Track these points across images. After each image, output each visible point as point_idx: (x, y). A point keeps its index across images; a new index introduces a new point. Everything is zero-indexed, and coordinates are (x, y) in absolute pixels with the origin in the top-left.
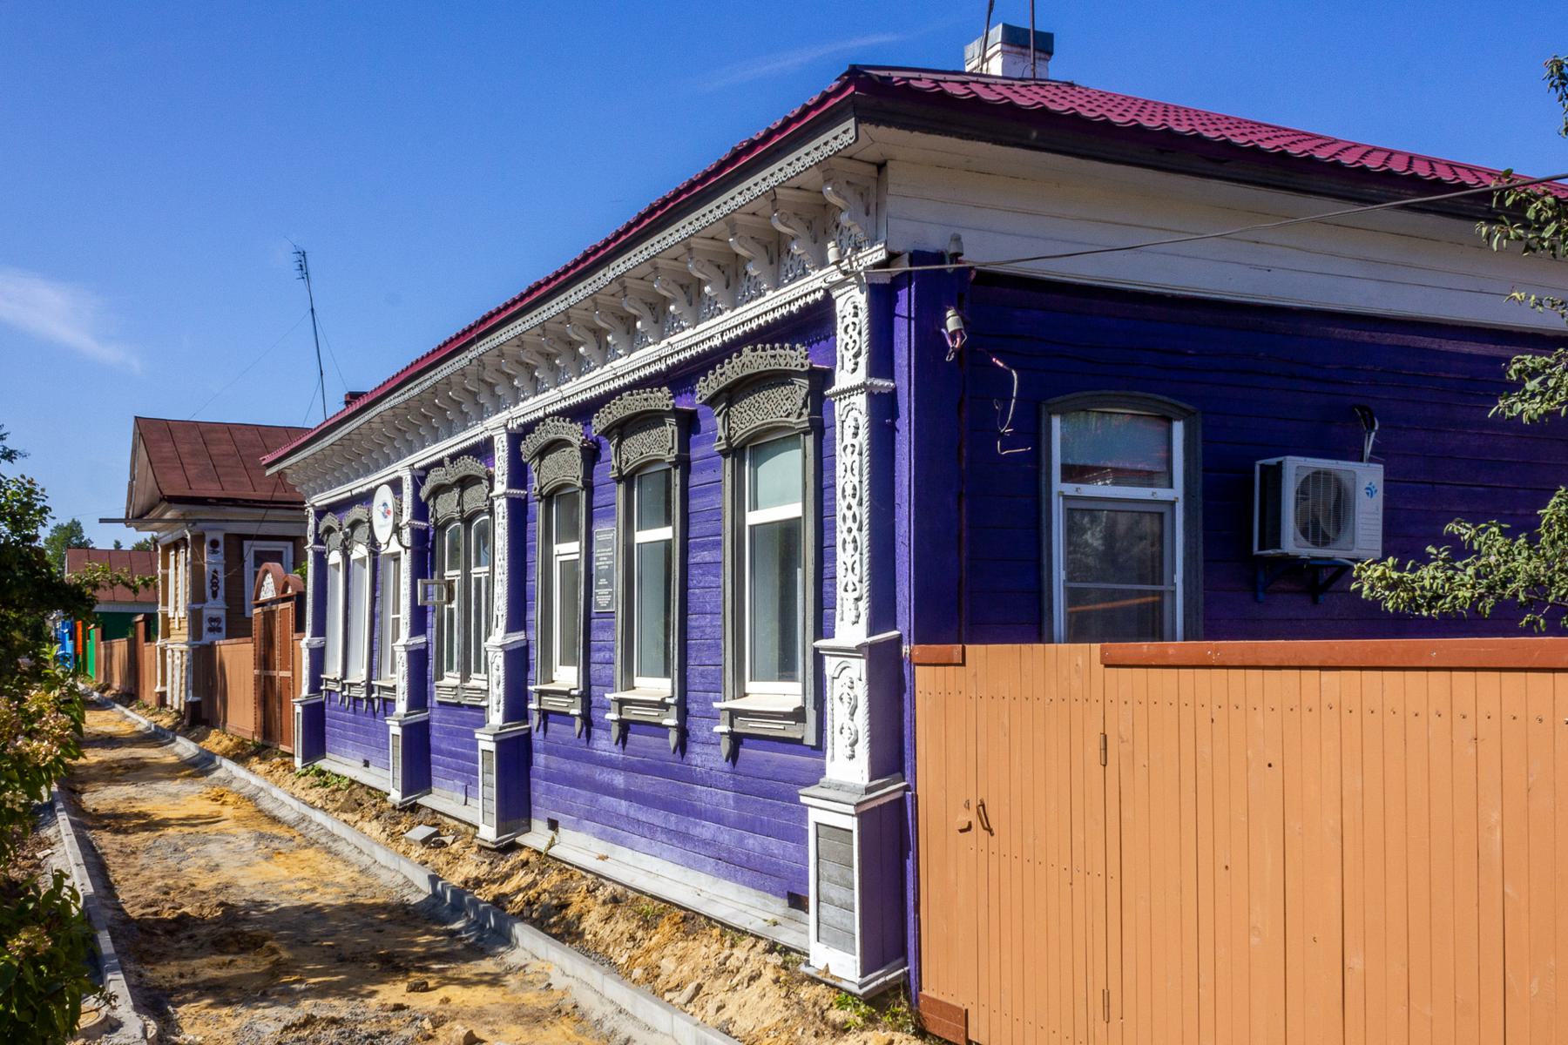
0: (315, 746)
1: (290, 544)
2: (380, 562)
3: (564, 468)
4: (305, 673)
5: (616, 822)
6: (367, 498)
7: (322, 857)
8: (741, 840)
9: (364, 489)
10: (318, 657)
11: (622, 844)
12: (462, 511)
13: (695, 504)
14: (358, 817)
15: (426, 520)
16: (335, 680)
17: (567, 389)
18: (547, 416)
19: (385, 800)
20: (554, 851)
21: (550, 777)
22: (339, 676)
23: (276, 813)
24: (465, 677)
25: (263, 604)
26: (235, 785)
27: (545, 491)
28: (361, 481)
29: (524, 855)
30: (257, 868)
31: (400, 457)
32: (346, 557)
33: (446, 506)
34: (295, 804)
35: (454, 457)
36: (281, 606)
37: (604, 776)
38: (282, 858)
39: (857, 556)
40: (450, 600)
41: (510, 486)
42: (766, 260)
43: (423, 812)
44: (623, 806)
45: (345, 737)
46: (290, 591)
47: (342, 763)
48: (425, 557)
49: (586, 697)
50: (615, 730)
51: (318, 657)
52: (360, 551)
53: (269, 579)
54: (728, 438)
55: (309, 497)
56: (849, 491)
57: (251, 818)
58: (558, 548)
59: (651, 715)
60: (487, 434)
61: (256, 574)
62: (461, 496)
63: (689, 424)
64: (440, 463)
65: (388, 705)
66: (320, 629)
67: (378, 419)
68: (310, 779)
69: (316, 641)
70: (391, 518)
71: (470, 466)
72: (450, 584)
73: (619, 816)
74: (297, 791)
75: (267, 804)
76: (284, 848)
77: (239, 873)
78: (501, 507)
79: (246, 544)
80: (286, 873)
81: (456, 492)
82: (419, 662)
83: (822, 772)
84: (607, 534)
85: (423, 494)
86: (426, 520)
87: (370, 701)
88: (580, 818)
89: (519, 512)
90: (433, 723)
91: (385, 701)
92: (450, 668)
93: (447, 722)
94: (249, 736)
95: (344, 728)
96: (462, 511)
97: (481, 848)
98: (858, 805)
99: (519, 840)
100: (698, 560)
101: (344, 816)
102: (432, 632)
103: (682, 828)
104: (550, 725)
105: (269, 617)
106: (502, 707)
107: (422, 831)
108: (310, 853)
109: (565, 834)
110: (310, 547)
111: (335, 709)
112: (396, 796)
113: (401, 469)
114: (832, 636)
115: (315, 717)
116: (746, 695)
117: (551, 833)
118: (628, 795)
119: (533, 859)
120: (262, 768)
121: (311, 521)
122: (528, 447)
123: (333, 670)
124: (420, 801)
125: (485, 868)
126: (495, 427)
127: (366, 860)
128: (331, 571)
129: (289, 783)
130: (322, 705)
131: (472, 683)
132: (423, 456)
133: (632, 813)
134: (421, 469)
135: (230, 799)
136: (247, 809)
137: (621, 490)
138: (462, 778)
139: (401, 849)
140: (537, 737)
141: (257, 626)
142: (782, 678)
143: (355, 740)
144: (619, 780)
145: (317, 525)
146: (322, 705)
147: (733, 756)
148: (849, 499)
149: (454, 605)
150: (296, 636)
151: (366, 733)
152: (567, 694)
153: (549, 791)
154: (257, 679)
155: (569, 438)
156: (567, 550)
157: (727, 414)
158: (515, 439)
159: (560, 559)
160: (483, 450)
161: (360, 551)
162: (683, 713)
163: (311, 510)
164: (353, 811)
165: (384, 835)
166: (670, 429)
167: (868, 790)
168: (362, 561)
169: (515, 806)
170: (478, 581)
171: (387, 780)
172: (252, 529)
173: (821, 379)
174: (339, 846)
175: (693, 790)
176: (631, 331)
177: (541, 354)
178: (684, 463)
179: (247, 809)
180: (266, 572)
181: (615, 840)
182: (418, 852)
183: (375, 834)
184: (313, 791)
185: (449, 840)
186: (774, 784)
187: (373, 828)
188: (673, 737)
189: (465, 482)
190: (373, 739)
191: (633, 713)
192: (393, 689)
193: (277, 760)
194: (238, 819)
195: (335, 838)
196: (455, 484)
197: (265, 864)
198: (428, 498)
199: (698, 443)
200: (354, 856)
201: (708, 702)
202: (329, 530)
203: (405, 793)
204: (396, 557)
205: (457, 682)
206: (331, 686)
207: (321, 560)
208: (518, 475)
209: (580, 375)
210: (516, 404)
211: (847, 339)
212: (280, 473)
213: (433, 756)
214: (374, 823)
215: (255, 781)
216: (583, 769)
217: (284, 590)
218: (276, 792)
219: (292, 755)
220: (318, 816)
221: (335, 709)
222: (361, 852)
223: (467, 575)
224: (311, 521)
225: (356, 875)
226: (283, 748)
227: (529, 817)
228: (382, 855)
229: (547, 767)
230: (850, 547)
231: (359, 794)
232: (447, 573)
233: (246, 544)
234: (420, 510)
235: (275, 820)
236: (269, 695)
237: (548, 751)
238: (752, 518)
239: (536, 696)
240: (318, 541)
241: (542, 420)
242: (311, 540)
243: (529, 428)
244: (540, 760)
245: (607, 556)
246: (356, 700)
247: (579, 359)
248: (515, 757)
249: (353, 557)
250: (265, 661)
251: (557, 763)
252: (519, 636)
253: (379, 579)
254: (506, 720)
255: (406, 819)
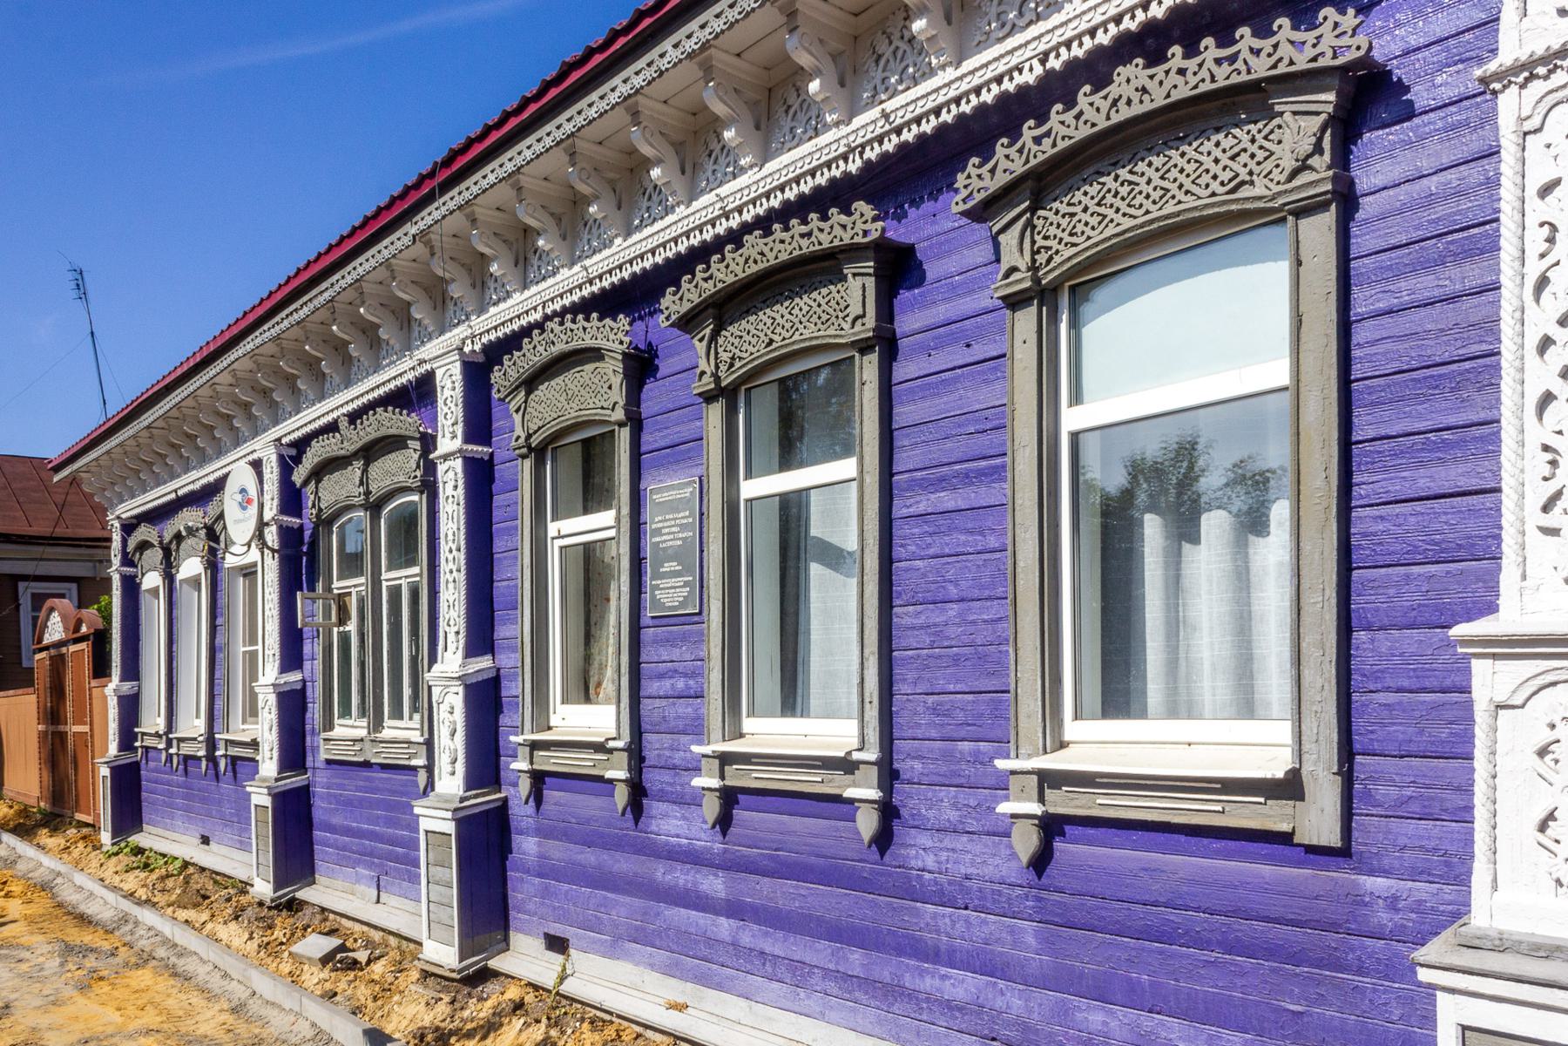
0: (128, 815)
1: (74, 586)
2: (223, 576)
3: (596, 393)
4: (113, 726)
5: (706, 952)
6: (217, 487)
7: (165, 983)
8: (1063, 1014)
10: (130, 708)
11: (720, 987)
12: (368, 493)
13: (904, 413)
14: (205, 916)
15: (299, 516)
16: (157, 735)
17: (598, 262)
18: (547, 318)
19: (244, 892)
20: (569, 987)
21: (546, 871)
22: (162, 728)
23: (83, 908)
24: (377, 725)
25: (47, 648)
26: (21, 867)
27: (534, 441)
28: (194, 475)
29: (513, 993)
30: (69, 1010)
31: (256, 433)
32: (169, 577)
33: (340, 488)
34: (111, 897)
35: (354, 417)
36: (73, 648)
37: (680, 876)
38: (104, 988)
40: (342, 620)
41: (468, 439)
43: (308, 911)
44: (724, 927)
45: (170, 806)
46: (84, 629)
47: (168, 838)
48: (300, 560)
49: (636, 754)
50: (711, 808)
51: (130, 708)
52: (191, 567)
53: (55, 618)
54: (1034, 268)
55: (113, 506)
57: (51, 918)
59: (582, 762)
60: (421, 370)
61: (35, 619)
62: (365, 471)
63: (898, 268)
64: (332, 427)
65: (242, 765)
66: (132, 670)
68: (126, 859)
69: (127, 687)
70: (253, 510)
73: (712, 942)
74: (108, 873)
75: (68, 895)
76: (105, 967)
77: (43, 1021)
78: (451, 477)
79: (22, 585)
80: (116, 1017)
81: (358, 464)
82: (293, 705)
83: (1459, 911)
84: (670, 492)
85: (298, 476)
86: (299, 516)
87: (212, 759)
88: (617, 938)
89: (481, 477)
90: (318, 789)
91: (234, 760)
92: (346, 712)
93: (341, 787)
94: (33, 802)
95: (171, 794)
96: (368, 493)
97: (426, 975)
98: (455, 810)
99: (494, 963)
100: (905, 512)
101: (182, 914)
102: (313, 667)
103: (886, 976)
104: (548, 794)
105: (58, 663)
106: (276, 754)
107: (316, 945)
108: (144, 977)
109: (579, 959)
111: (157, 770)
112: (263, 888)
113: (264, 447)
114: (1491, 608)
115: (127, 783)
116: (742, 736)
117: (560, 958)
118: (734, 909)
119: (530, 998)
120: (54, 842)
121: (117, 538)
122: (502, 377)
123: (152, 721)
124: (299, 895)
125: (442, 1009)
126: (441, 356)
127: (241, 993)
128: (145, 601)
129: (95, 864)
130: (136, 766)
131: (387, 734)
132: (294, 426)
133: (746, 939)
134: (293, 444)
135: (16, 888)
136: (41, 905)
137: (714, 414)
138: (370, 866)
139: (286, 968)
140: (521, 811)
141: (42, 676)
142: (783, 714)
143: (187, 810)
144: (714, 884)
146: (136, 766)
147: (724, 822)
149: (352, 627)
150: (94, 683)
151: (204, 800)
152: (599, 748)
153: (546, 893)
154: (43, 736)
155: (600, 343)
156: (574, 528)
157: (1030, 225)
158: (477, 373)
160: (418, 394)
161: (191, 567)
162: (889, 774)
163: (117, 524)
164: (196, 906)
165: (252, 946)
166: (857, 290)
167: (462, 800)
168: (195, 582)
169: (486, 910)
170: (395, 592)
171: (249, 863)
174: (188, 965)
175: (917, 913)
178: (886, 344)
179: (41, 905)
180: (52, 610)
181: (703, 980)
182: (314, 976)
183: (237, 942)
184: (131, 876)
185: (362, 956)
186: (1173, 915)
187: (233, 933)
188: (621, 795)
190: (393, 860)
191: (738, 777)
192: (254, 744)
193: (72, 832)
194: (30, 920)
195: (183, 953)
196: (355, 455)
197: (81, 1000)
198: (306, 483)
199: (912, 306)
200: (216, 982)
201: (986, 761)
202: (144, 546)
203: (278, 885)
204: (249, 572)
205: (363, 733)
206: (149, 742)
207: (131, 586)
208: (479, 424)
209: (628, 234)
210: (482, 310)
212: (74, 481)
213: (317, 834)
214: (233, 925)
215: (48, 862)
216: (624, 864)
217: (77, 629)
218: (79, 878)
219: (94, 827)
220: (147, 916)
221: (157, 770)
222: (226, 975)
224: (117, 538)
225: (225, 1017)
226: (80, 816)
227: (506, 928)
228: (264, 984)
229: (541, 856)
231: (199, 882)
232: (336, 584)
233: (22, 585)
234: (291, 499)
235: (84, 920)
236: (59, 754)
237: (543, 833)
238: (1072, 419)
239: (524, 752)
240: (127, 561)
241: (539, 325)
242: (116, 561)
244: (526, 846)
245: (668, 528)
246: (187, 759)
248: (485, 843)
249: (179, 577)
250: (53, 715)
251: (559, 851)
252: (484, 663)
254: (469, 786)
255: (282, 926)
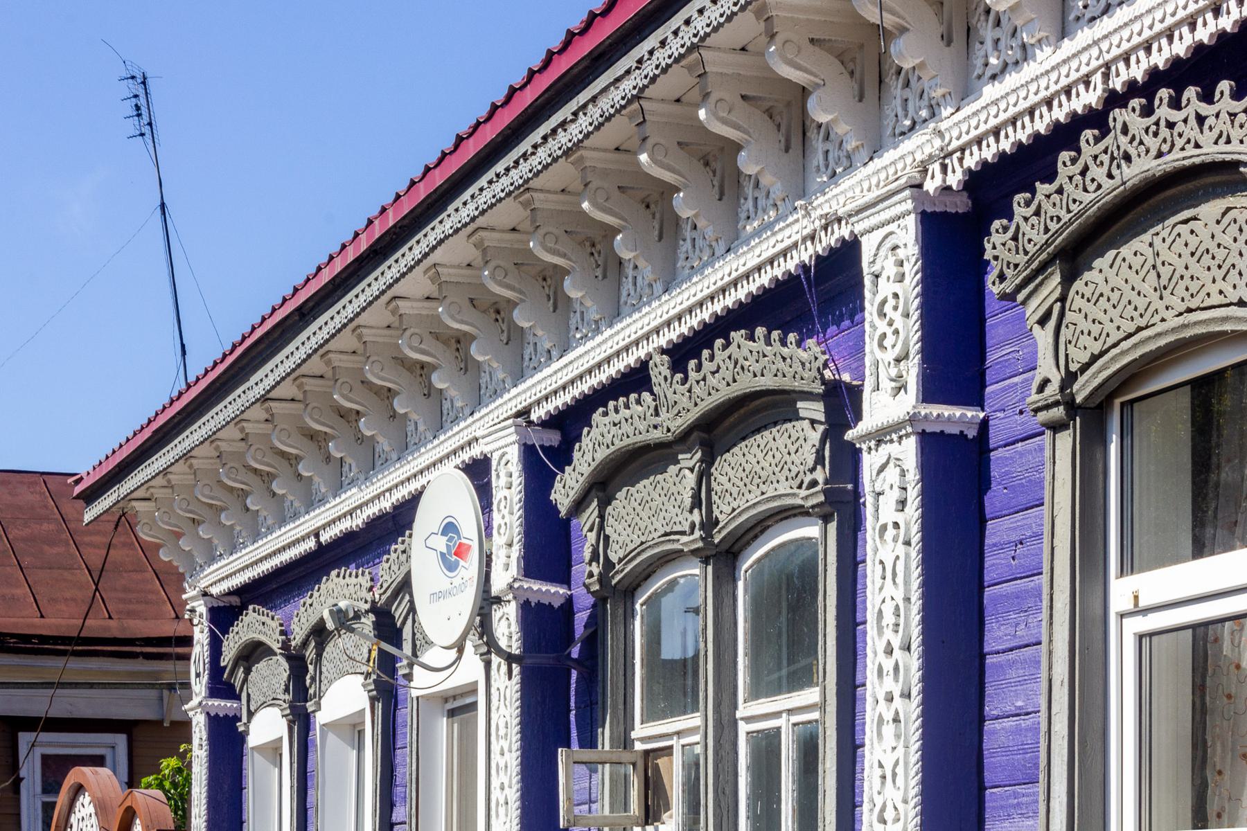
9: (386, 504)
12: (710, 524)
15: (565, 580)
18: (1114, 100)
27: (1082, 390)
28: (353, 497)
32: (301, 720)
33: (651, 513)
35: (683, 354)
39: (900, 751)
41: (930, 393)
42: (715, 193)
52: (344, 696)
55: (195, 569)
56: (889, 619)
58: (1121, 592)
62: (704, 475)
67: (304, 374)
71: (756, 362)
72: (650, 766)
81: (690, 460)
86: (565, 580)
89: (958, 479)
96: (710, 524)
110: (198, 707)
121: (201, 636)
132: (554, 382)
145: (216, 647)
148: (889, 634)
159: (1136, 625)
160: (821, 294)
161: (344, 696)
170: (766, 747)
172: (319, 522)
173: (842, 402)
176: (669, 228)
177: (437, 336)
180: (79, 789)
189: (718, 431)
196: (683, 440)
198: (579, 505)
202: (253, 653)
204: (459, 706)
207: (228, 738)
208: (956, 352)
211: (882, 326)
212: (122, 519)
223: (725, 726)
230: (889, 730)
234: (548, 545)
240: (221, 686)
241: (1096, 119)
242: (199, 687)
243: (571, 421)
247: (367, 444)
253: (404, 772)
